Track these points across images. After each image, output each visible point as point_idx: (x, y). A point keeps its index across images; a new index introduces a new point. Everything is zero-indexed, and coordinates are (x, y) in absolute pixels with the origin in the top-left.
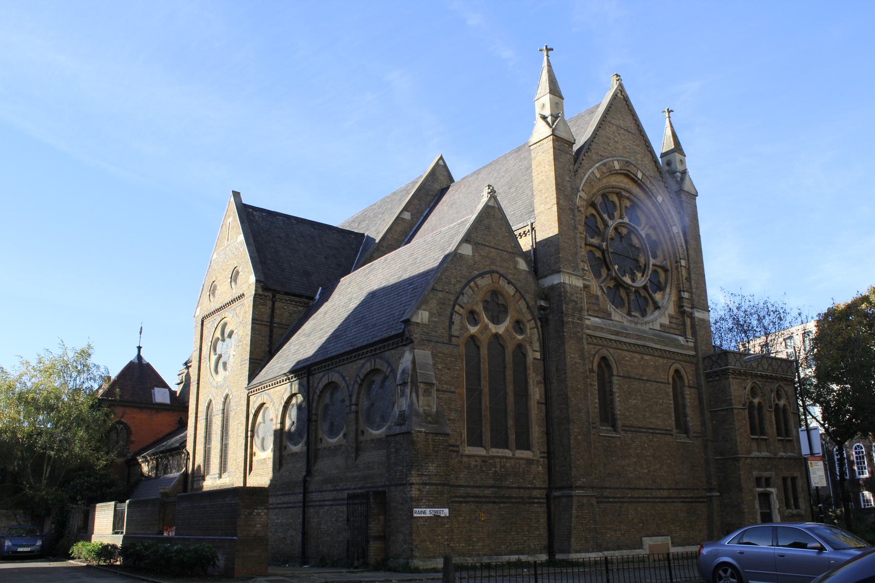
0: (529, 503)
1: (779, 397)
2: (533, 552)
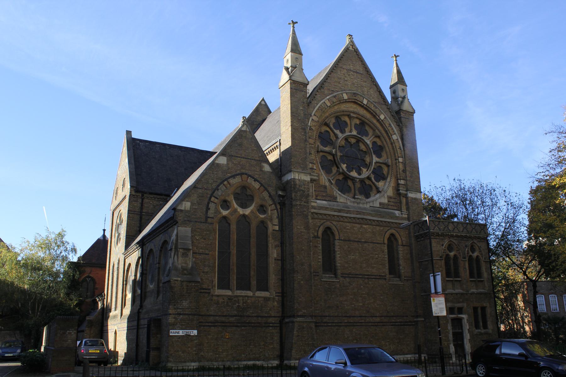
0: (264, 326)
1: (473, 250)
2: (266, 359)
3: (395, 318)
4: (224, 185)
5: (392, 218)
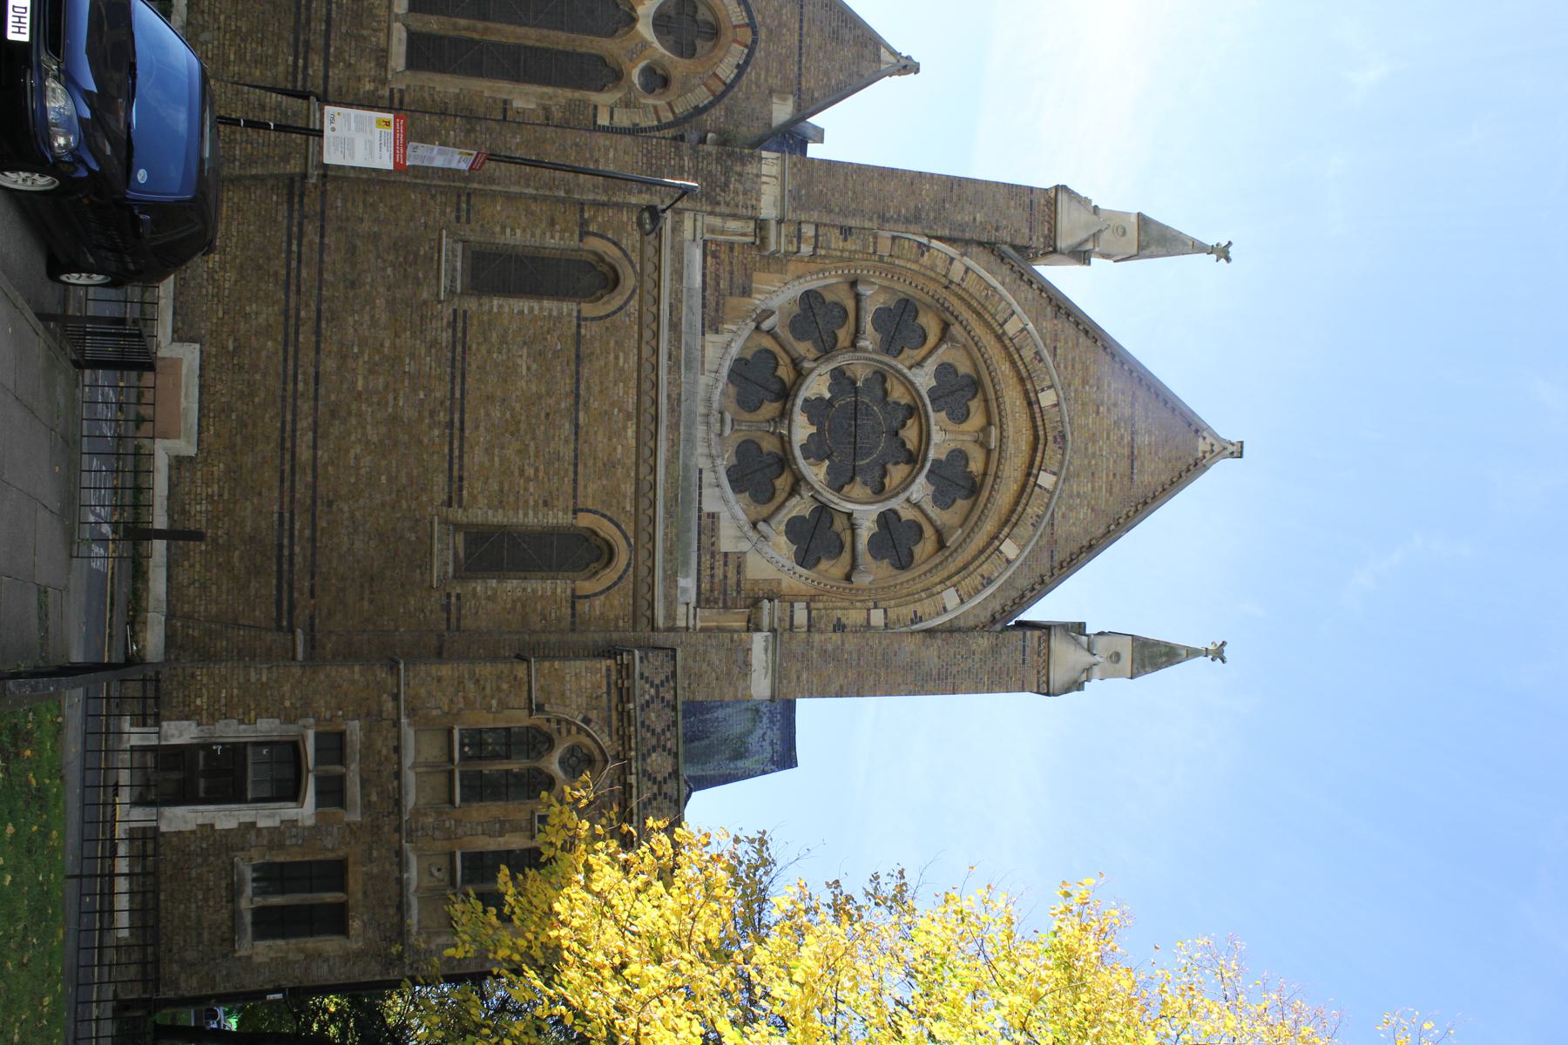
0: (296, 39)
3: (307, 533)
5: (669, 552)
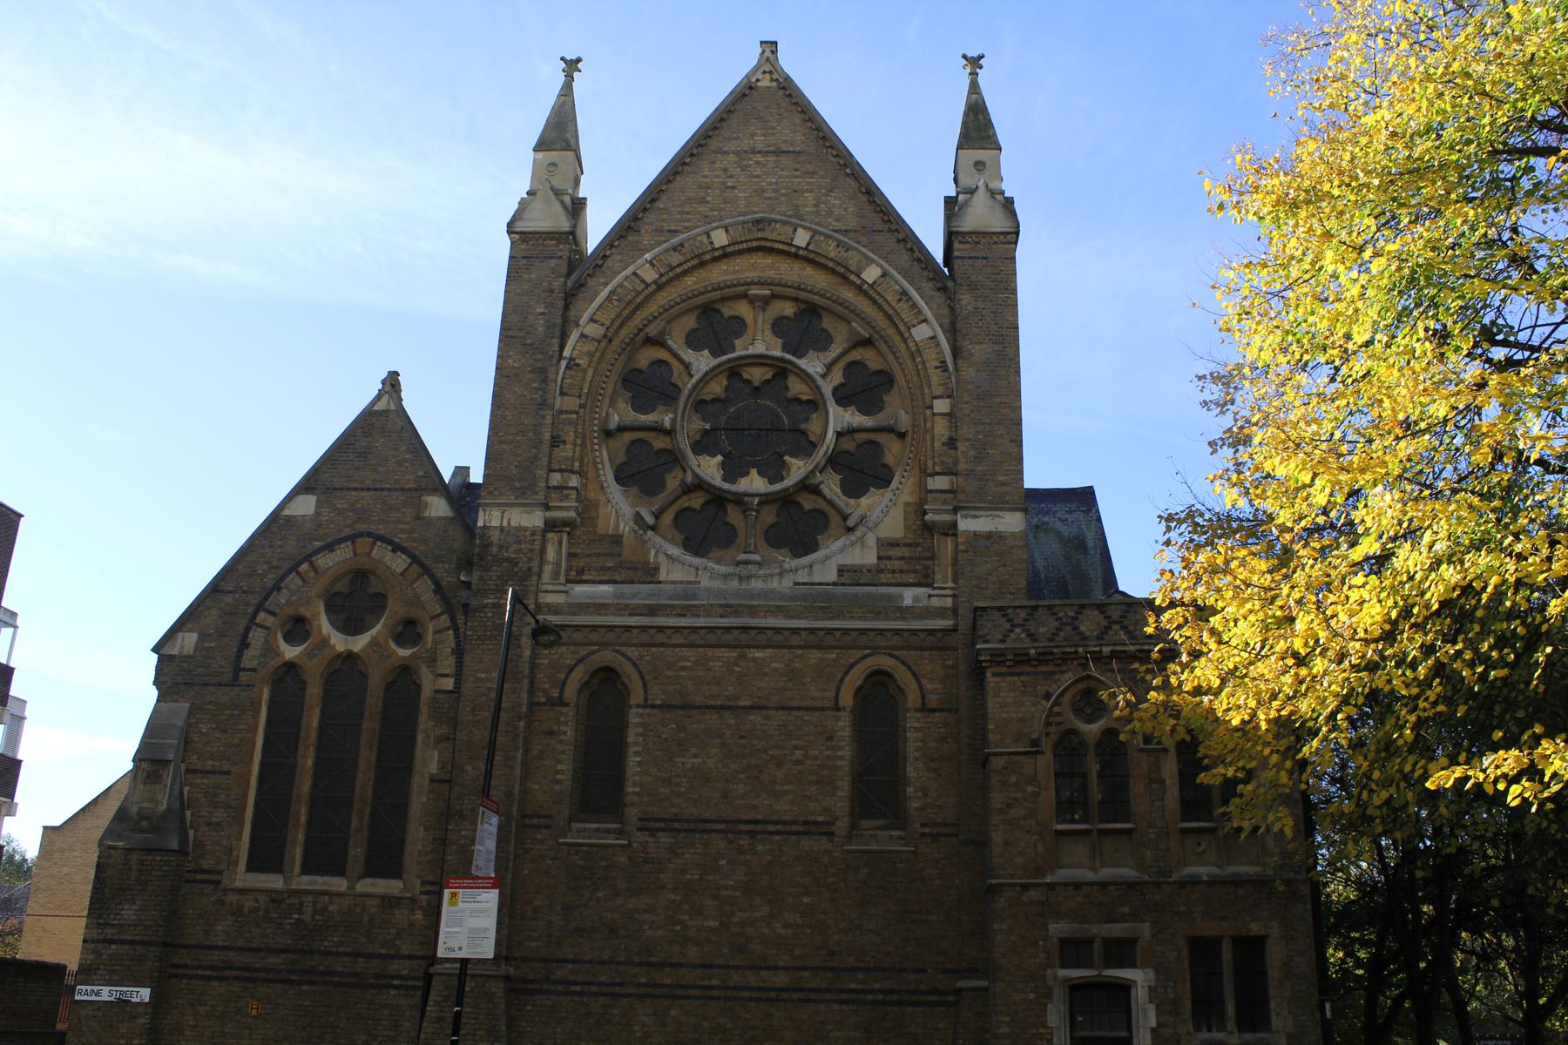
3: (860, 976)
4: (298, 573)
5: (877, 615)
